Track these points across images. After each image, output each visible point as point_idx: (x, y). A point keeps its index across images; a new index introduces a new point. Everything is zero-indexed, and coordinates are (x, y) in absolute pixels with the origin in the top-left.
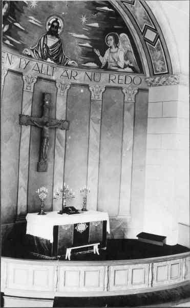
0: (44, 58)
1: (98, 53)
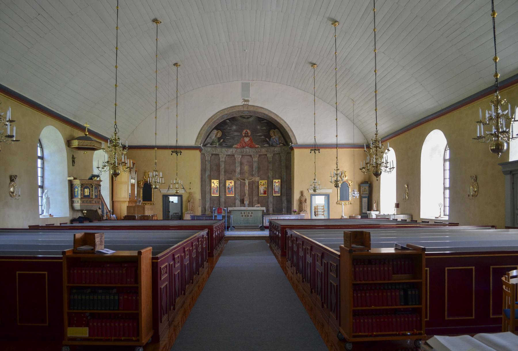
0: (244, 147)
1: (268, 140)
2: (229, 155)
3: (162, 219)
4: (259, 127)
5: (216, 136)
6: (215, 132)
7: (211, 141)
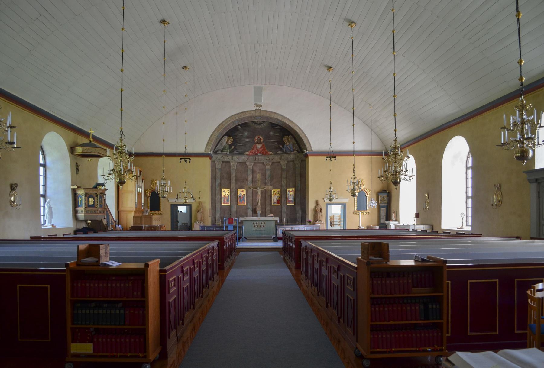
0: (256, 154)
1: (281, 146)
2: (240, 163)
3: (170, 229)
4: (272, 133)
5: (227, 143)
6: (226, 138)
7: (221, 148)
